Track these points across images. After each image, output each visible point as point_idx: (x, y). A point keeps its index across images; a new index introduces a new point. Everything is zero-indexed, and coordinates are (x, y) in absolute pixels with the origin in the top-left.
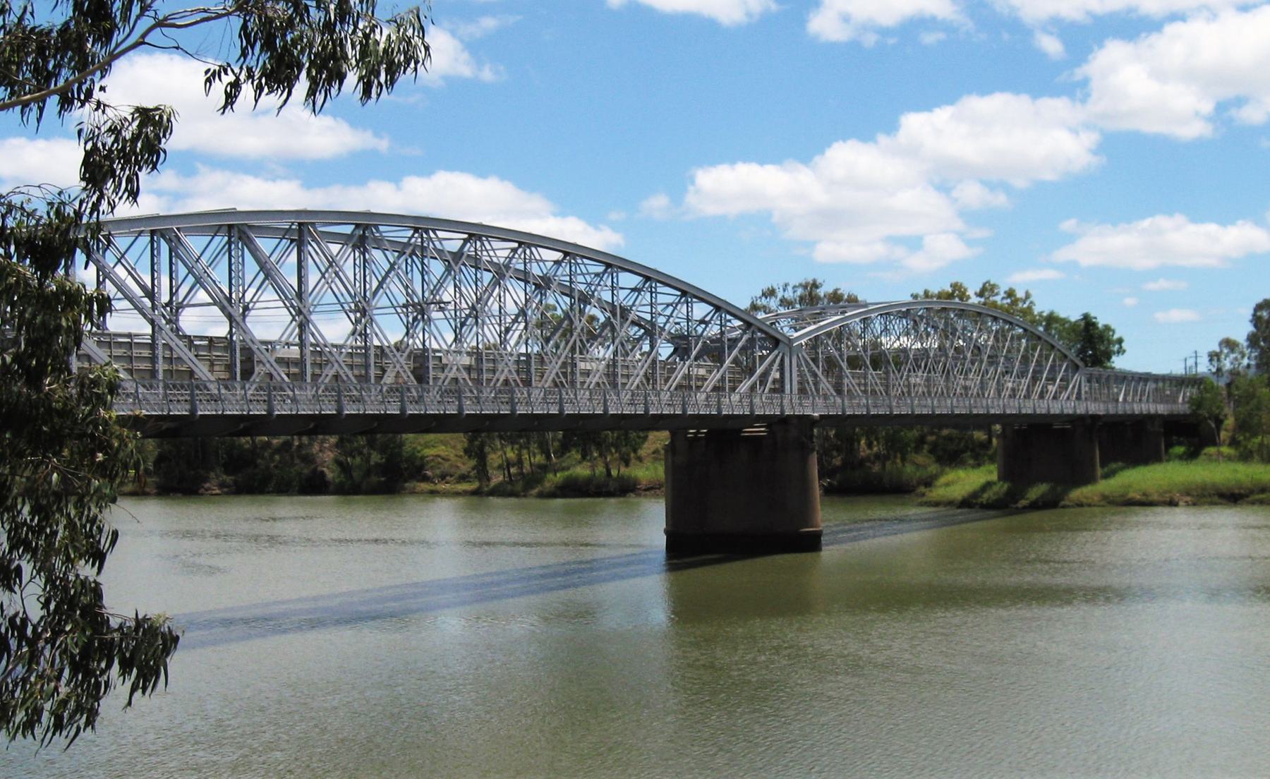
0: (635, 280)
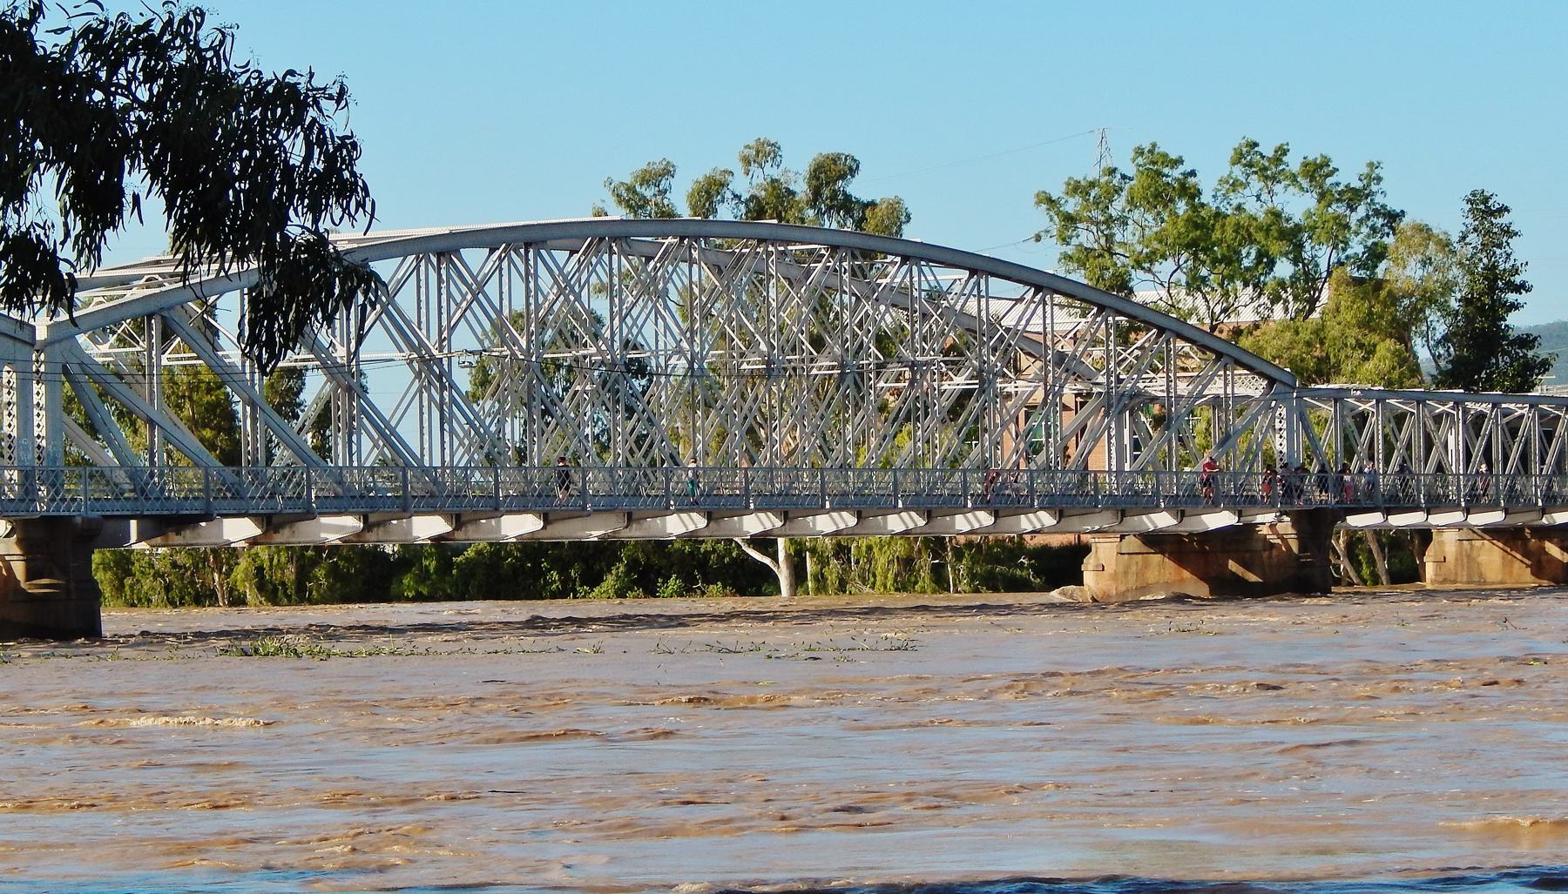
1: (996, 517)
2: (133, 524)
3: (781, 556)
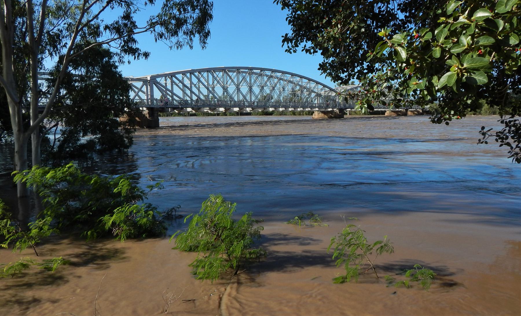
0: (307, 81)
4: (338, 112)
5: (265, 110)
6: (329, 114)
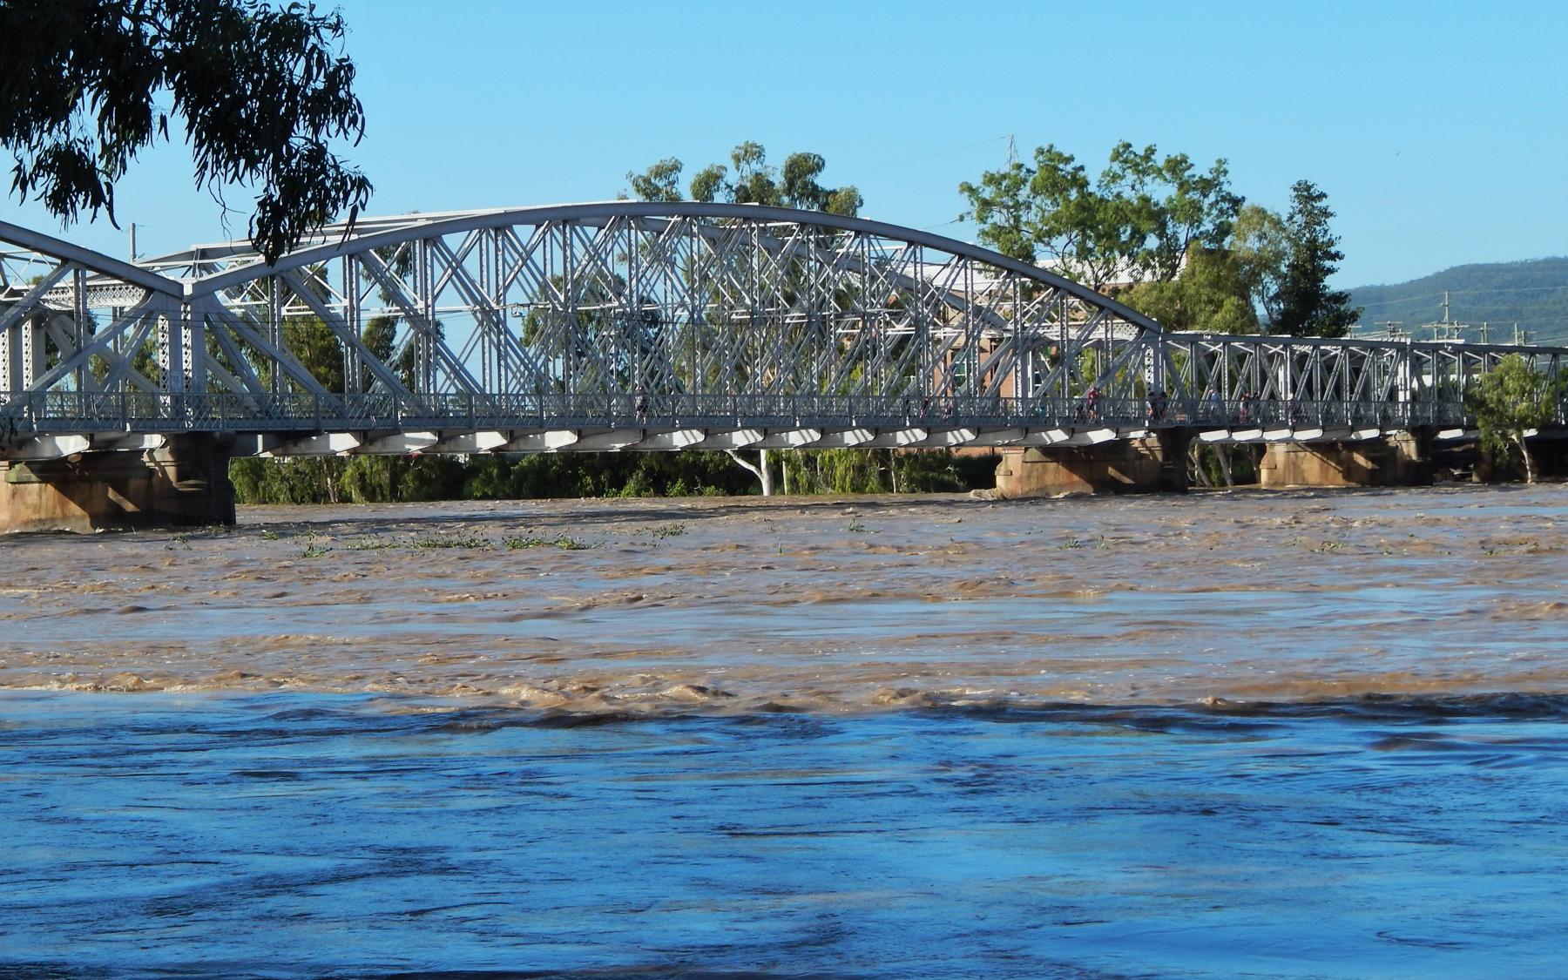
1: (706, 435)
2: (260, 437)
3: (763, 464)
4: (171, 472)
5: (513, 447)
6: (99, 486)
